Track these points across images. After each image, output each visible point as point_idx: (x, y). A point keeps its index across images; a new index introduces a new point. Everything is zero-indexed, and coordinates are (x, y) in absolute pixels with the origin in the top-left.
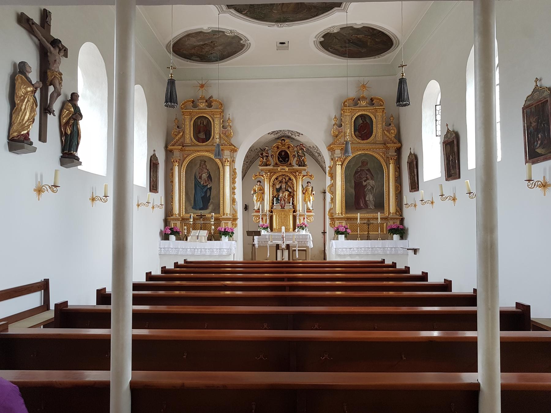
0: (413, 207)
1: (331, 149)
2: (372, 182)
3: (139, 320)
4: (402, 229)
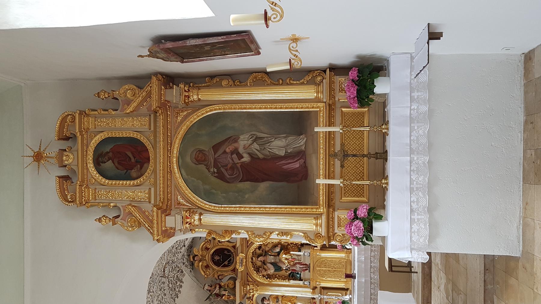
0: (300, 46)
1: (168, 234)
2: (244, 142)
3: (331, 124)
4: (359, 71)
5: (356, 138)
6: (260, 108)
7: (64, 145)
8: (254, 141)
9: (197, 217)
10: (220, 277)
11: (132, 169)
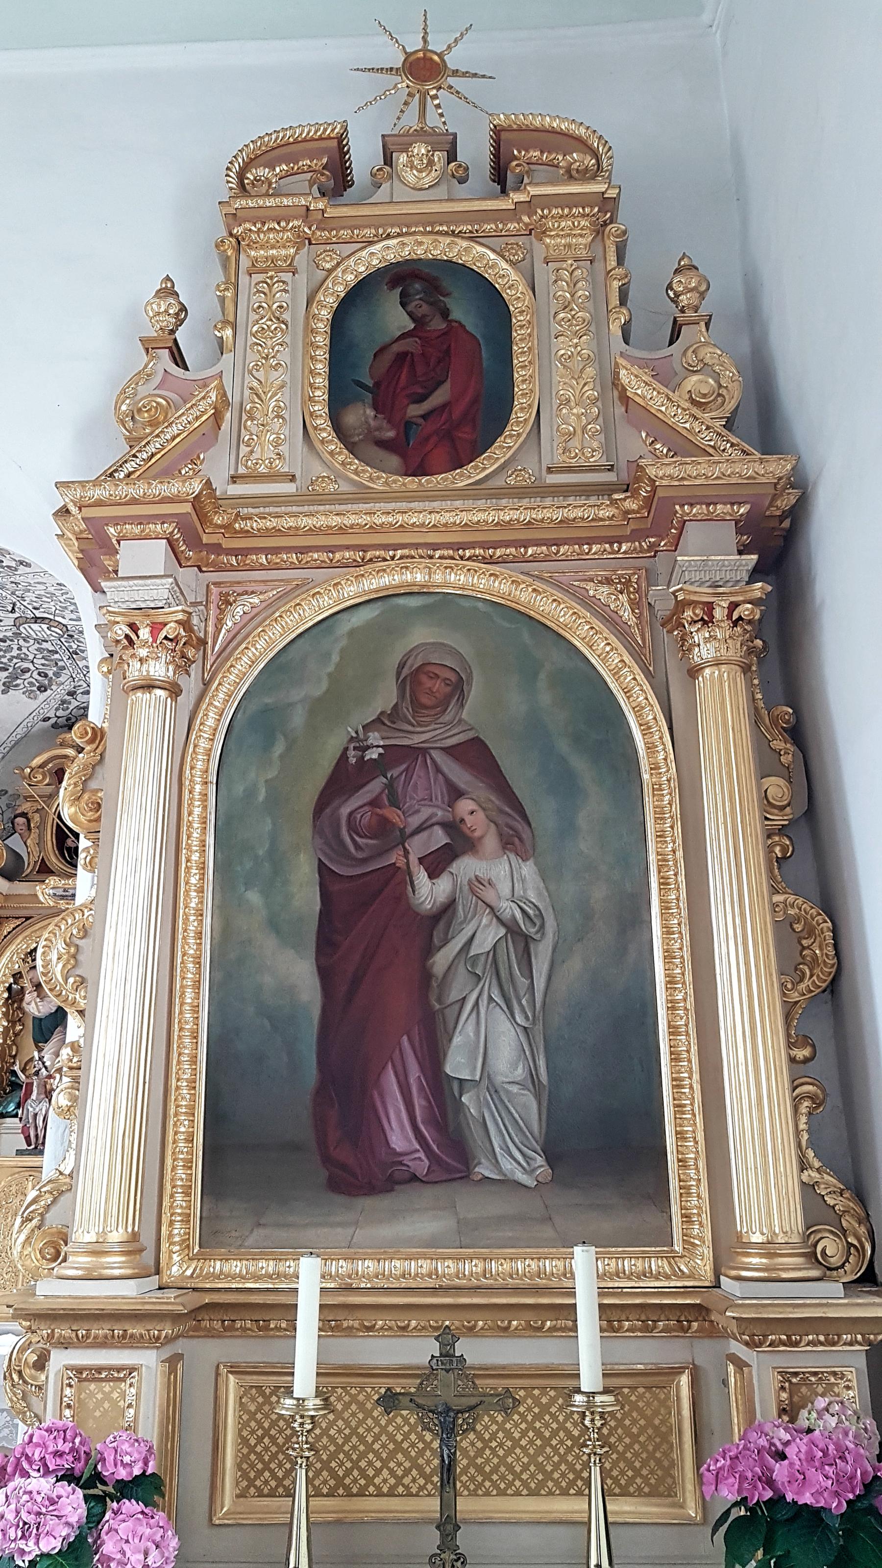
1: (96, 556)
2: (504, 879)
3: (611, 1316)
5: (540, 1450)
6: (669, 956)
7: (476, 150)
8: (512, 929)
9: (159, 670)
10: (20, 820)
11: (375, 407)
